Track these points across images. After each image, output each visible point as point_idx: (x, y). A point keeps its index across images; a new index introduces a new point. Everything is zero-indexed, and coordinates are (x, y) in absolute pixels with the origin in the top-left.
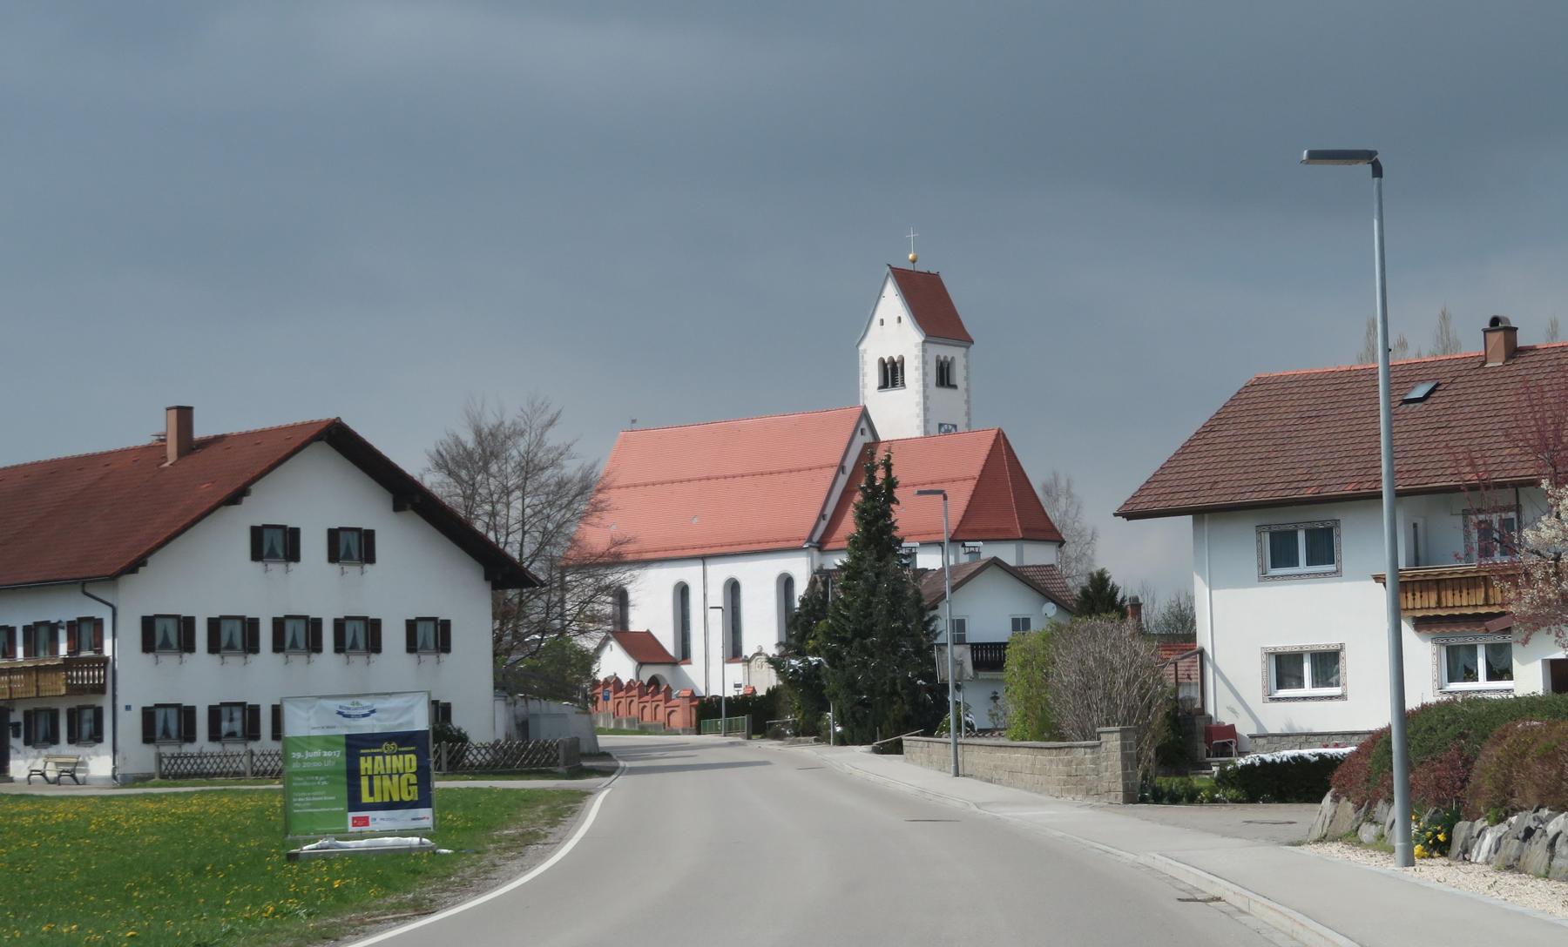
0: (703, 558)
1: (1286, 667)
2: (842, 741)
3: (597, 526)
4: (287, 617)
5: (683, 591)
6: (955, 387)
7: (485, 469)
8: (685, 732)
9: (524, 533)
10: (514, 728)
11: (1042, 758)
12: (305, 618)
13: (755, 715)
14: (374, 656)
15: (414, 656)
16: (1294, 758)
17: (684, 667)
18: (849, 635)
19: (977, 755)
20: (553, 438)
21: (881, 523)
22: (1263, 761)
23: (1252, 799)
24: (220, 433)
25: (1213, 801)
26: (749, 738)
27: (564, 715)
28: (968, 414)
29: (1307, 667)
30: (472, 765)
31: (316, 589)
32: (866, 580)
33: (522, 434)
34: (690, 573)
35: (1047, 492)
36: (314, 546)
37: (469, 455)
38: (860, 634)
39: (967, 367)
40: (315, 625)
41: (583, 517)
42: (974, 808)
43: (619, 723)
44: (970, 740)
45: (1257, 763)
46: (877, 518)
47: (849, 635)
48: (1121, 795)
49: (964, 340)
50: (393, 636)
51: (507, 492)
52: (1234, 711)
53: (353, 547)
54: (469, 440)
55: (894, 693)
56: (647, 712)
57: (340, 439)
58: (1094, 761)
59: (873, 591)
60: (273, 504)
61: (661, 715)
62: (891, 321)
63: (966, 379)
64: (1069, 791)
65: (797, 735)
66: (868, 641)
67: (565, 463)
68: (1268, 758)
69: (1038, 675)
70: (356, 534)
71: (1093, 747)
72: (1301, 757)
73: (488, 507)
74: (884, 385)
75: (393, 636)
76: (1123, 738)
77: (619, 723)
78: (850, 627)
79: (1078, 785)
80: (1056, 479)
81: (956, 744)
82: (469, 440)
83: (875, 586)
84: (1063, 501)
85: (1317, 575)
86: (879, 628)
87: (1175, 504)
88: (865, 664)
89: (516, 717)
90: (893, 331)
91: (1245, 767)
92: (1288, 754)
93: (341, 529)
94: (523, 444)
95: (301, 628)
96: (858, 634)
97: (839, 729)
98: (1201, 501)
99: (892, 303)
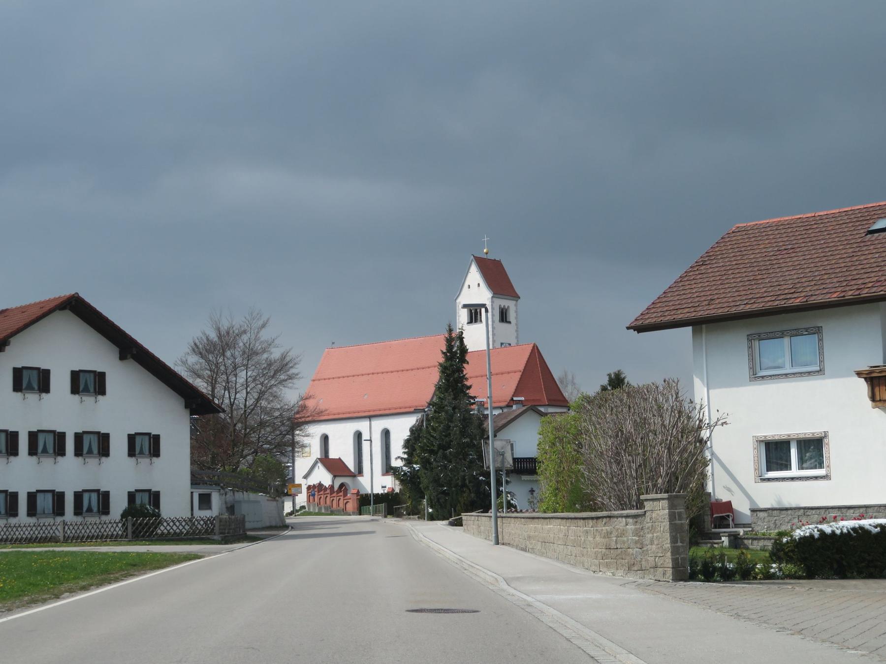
0: (370, 417)
1: (775, 453)
2: (432, 518)
3: (291, 388)
4: (39, 431)
5: (358, 436)
6: (510, 322)
7: (223, 354)
8: (354, 514)
9: (247, 393)
10: (224, 510)
11: (576, 530)
12: (53, 432)
13: (389, 504)
14: (104, 459)
15: (134, 459)
16: (854, 529)
17: (360, 478)
18: (435, 448)
19: (513, 527)
20: (265, 335)
21: (456, 375)
22: (822, 532)
23: (810, 575)
24: (4, 308)
25: (768, 576)
26: (385, 517)
27: (257, 502)
28: (517, 337)
29: (794, 452)
30: (163, 533)
31: (61, 411)
32: (447, 412)
33: (245, 332)
34: (363, 426)
35: (562, 382)
36: (60, 382)
37: (215, 345)
38: (444, 447)
39: (516, 312)
40: (60, 438)
41: (281, 382)
42: (504, 586)
43: (320, 509)
44: (508, 515)
45: (816, 534)
46: (454, 372)
47: (435, 448)
48: (670, 572)
49: (515, 297)
50: (119, 446)
51: (235, 368)
52: (729, 490)
53: (90, 384)
54: (213, 336)
55: (464, 485)
56: (334, 502)
57: (77, 307)
58: (636, 533)
59: (450, 419)
60: (28, 353)
61: (341, 505)
62: (474, 286)
63: (516, 318)
64: (608, 565)
65: (409, 515)
66: (448, 451)
67: (273, 350)
68: (827, 529)
69: (570, 448)
70: (92, 375)
71: (635, 516)
72: (861, 528)
73: (224, 377)
74: (470, 322)
75: (119, 446)
76: (672, 507)
77: (320, 509)
78: (436, 443)
79: (619, 558)
80: (566, 375)
81: (497, 517)
82: (213, 336)
83: (452, 416)
84: (570, 388)
85: (801, 374)
86: (455, 443)
87: (680, 316)
88: (445, 467)
89: (226, 503)
90: (475, 289)
91: (803, 539)
92: (848, 524)
93: (81, 371)
94: (245, 338)
95: (50, 439)
96: (441, 447)
97: (430, 510)
98: (702, 313)
99: (474, 276)
